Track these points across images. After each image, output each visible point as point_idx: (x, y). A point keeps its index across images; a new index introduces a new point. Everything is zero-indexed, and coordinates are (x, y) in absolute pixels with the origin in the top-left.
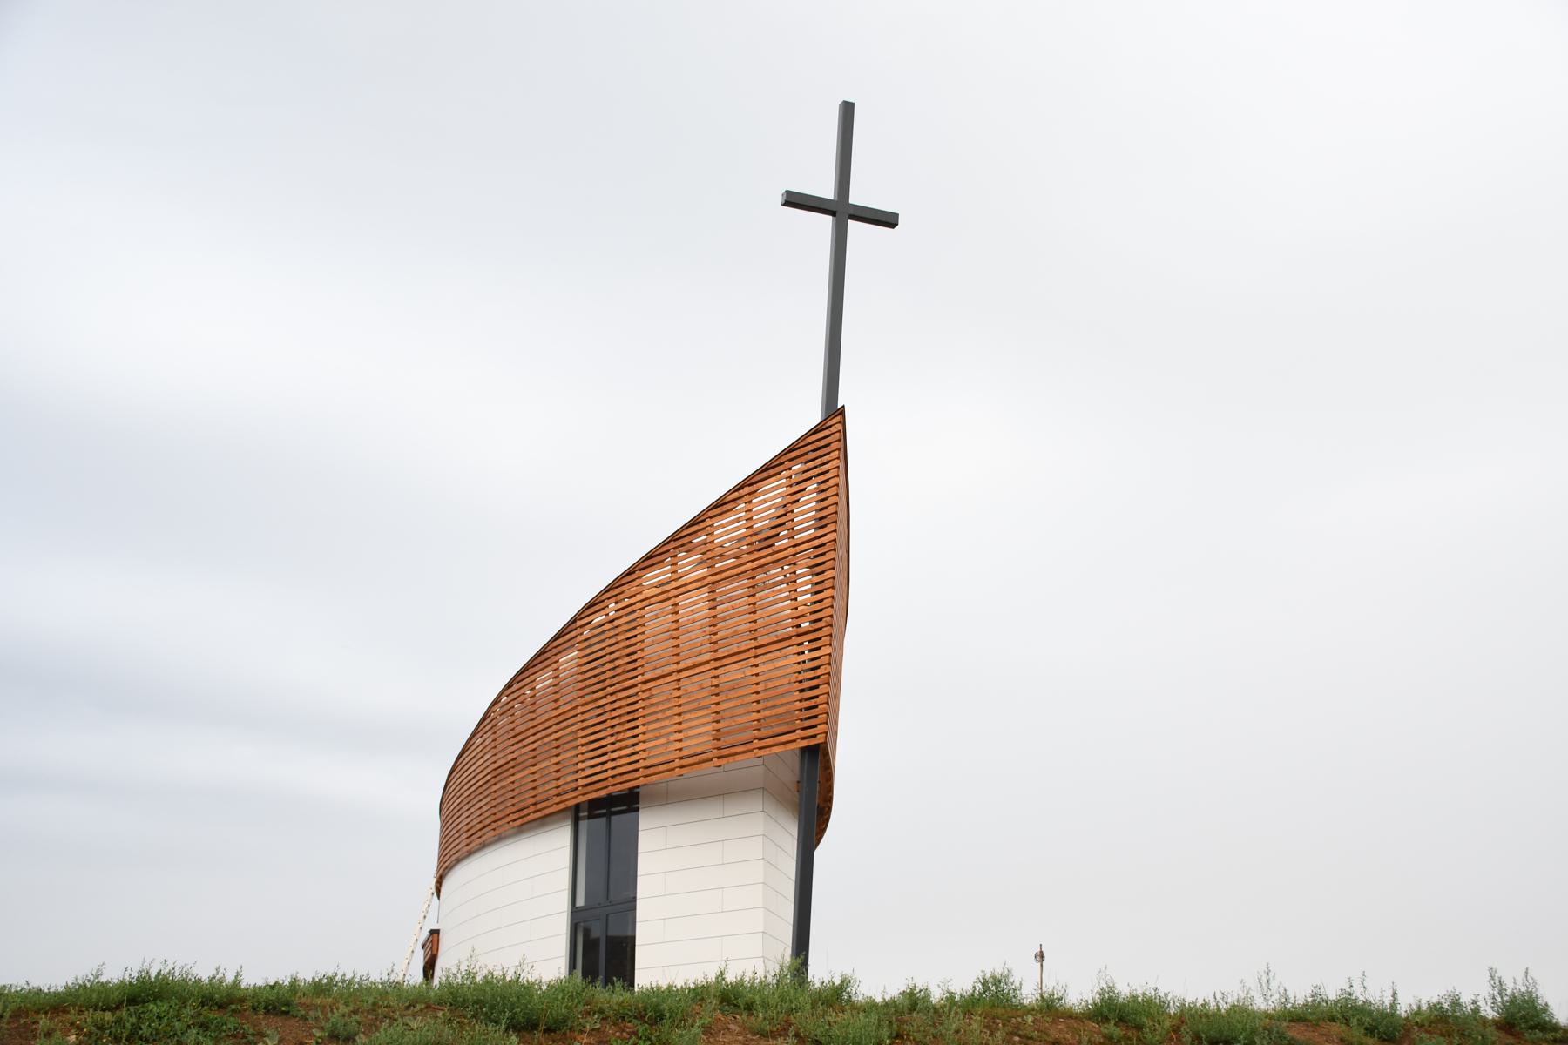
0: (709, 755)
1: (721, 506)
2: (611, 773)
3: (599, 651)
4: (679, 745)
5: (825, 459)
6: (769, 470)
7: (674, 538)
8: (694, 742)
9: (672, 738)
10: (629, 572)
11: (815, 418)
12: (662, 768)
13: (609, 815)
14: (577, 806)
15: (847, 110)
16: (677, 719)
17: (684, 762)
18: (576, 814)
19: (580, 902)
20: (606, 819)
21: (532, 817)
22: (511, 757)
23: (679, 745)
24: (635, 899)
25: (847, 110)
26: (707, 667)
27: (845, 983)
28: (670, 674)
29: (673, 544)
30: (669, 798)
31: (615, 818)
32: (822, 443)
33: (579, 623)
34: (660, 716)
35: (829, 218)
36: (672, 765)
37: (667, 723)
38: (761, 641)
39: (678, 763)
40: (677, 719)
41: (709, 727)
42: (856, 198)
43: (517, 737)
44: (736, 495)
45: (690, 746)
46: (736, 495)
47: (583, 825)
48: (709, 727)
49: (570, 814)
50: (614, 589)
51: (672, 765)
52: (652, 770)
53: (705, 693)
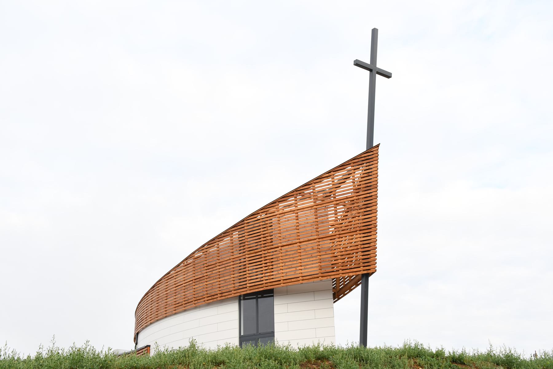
0: (318, 276)
1: (319, 179)
2: (265, 282)
3: (254, 232)
4: (301, 271)
5: (371, 163)
6: (342, 166)
7: (296, 190)
8: (309, 270)
9: (298, 268)
10: (274, 202)
11: (365, 149)
12: (293, 280)
13: (257, 298)
14: (240, 296)
15: (375, 32)
16: (300, 261)
17: (304, 278)
18: (241, 298)
19: (242, 334)
20: (257, 300)
21: (219, 299)
22: (206, 274)
23: (301, 271)
24: (273, 333)
25: (375, 32)
26: (315, 241)
27: (193, 345)
28: (315, 239)
29: (295, 193)
30: (288, 293)
31: (259, 299)
32: (370, 157)
33: (246, 222)
34: (291, 260)
35: (369, 72)
36: (299, 279)
37: (295, 262)
38: (301, 240)
39: (301, 278)
40: (300, 261)
41: (318, 265)
42: (380, 65)
43: (209, 267)
44: (327, 175)
45: (306, 272)
46: (327, 175)
47: (242, 302)
48: (318, 265)
49: (238, 298)
50: (264, 209)
51: (299, 279)
52: (304, 278)
53: (315, 251)
